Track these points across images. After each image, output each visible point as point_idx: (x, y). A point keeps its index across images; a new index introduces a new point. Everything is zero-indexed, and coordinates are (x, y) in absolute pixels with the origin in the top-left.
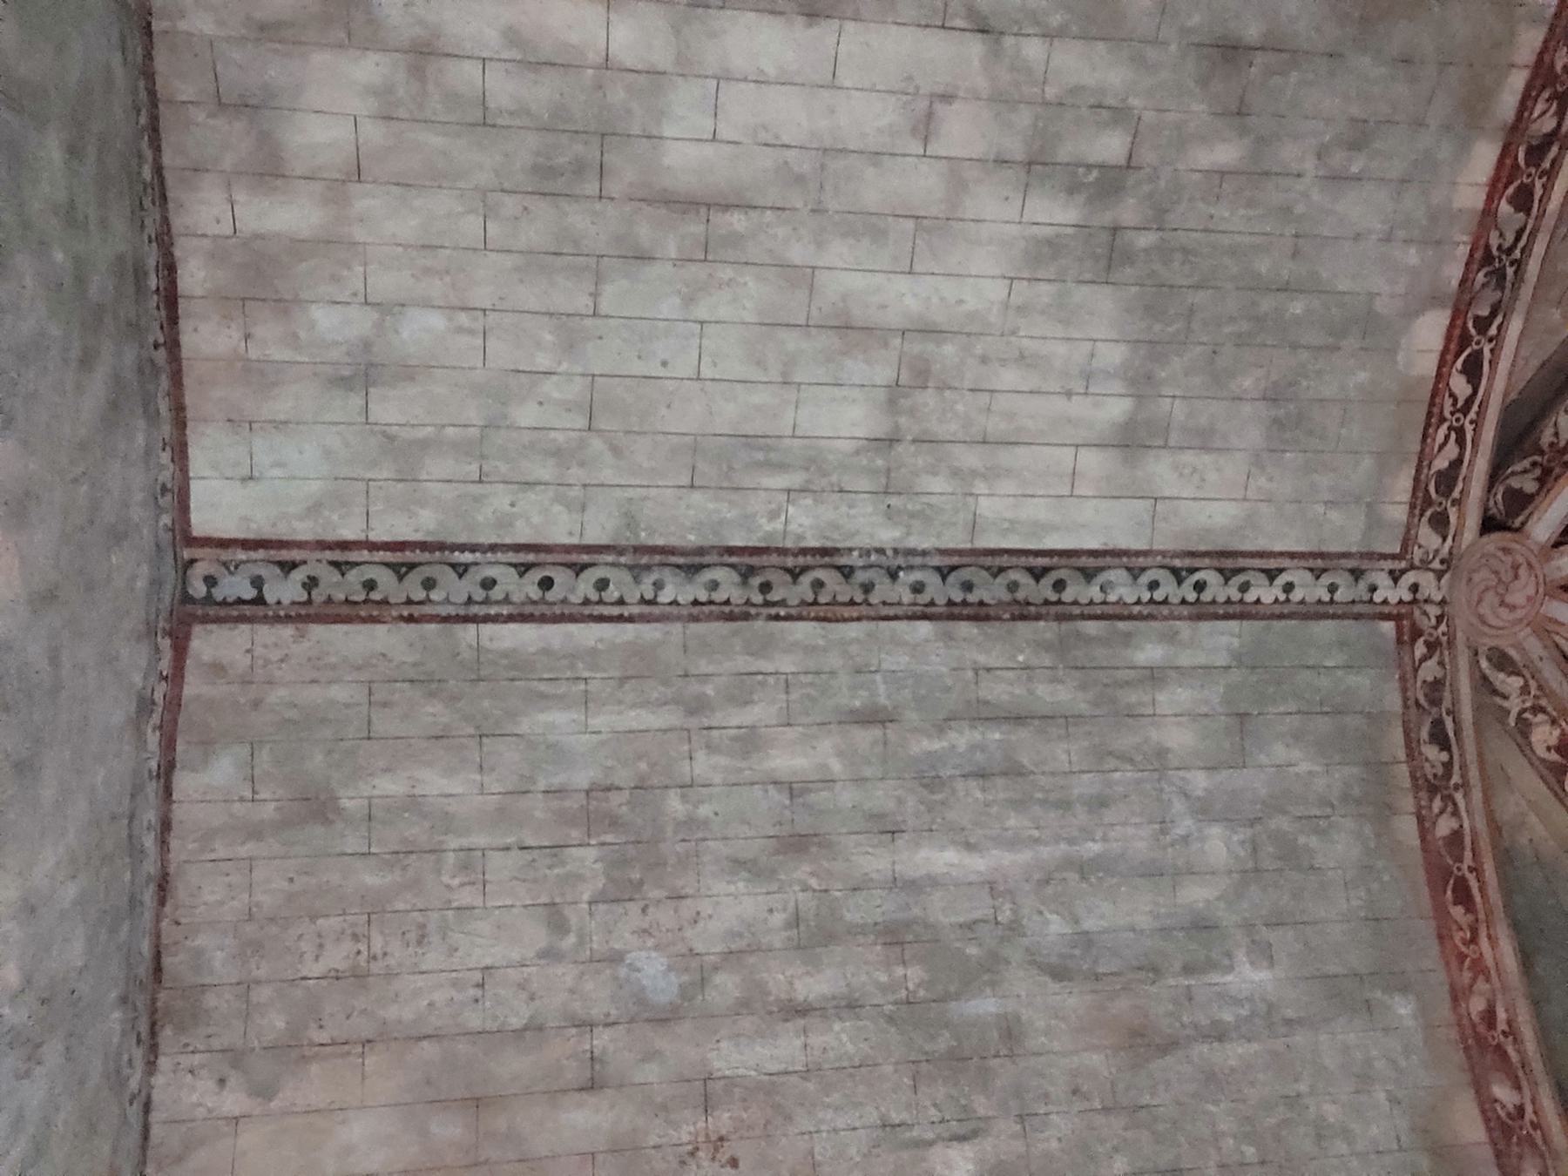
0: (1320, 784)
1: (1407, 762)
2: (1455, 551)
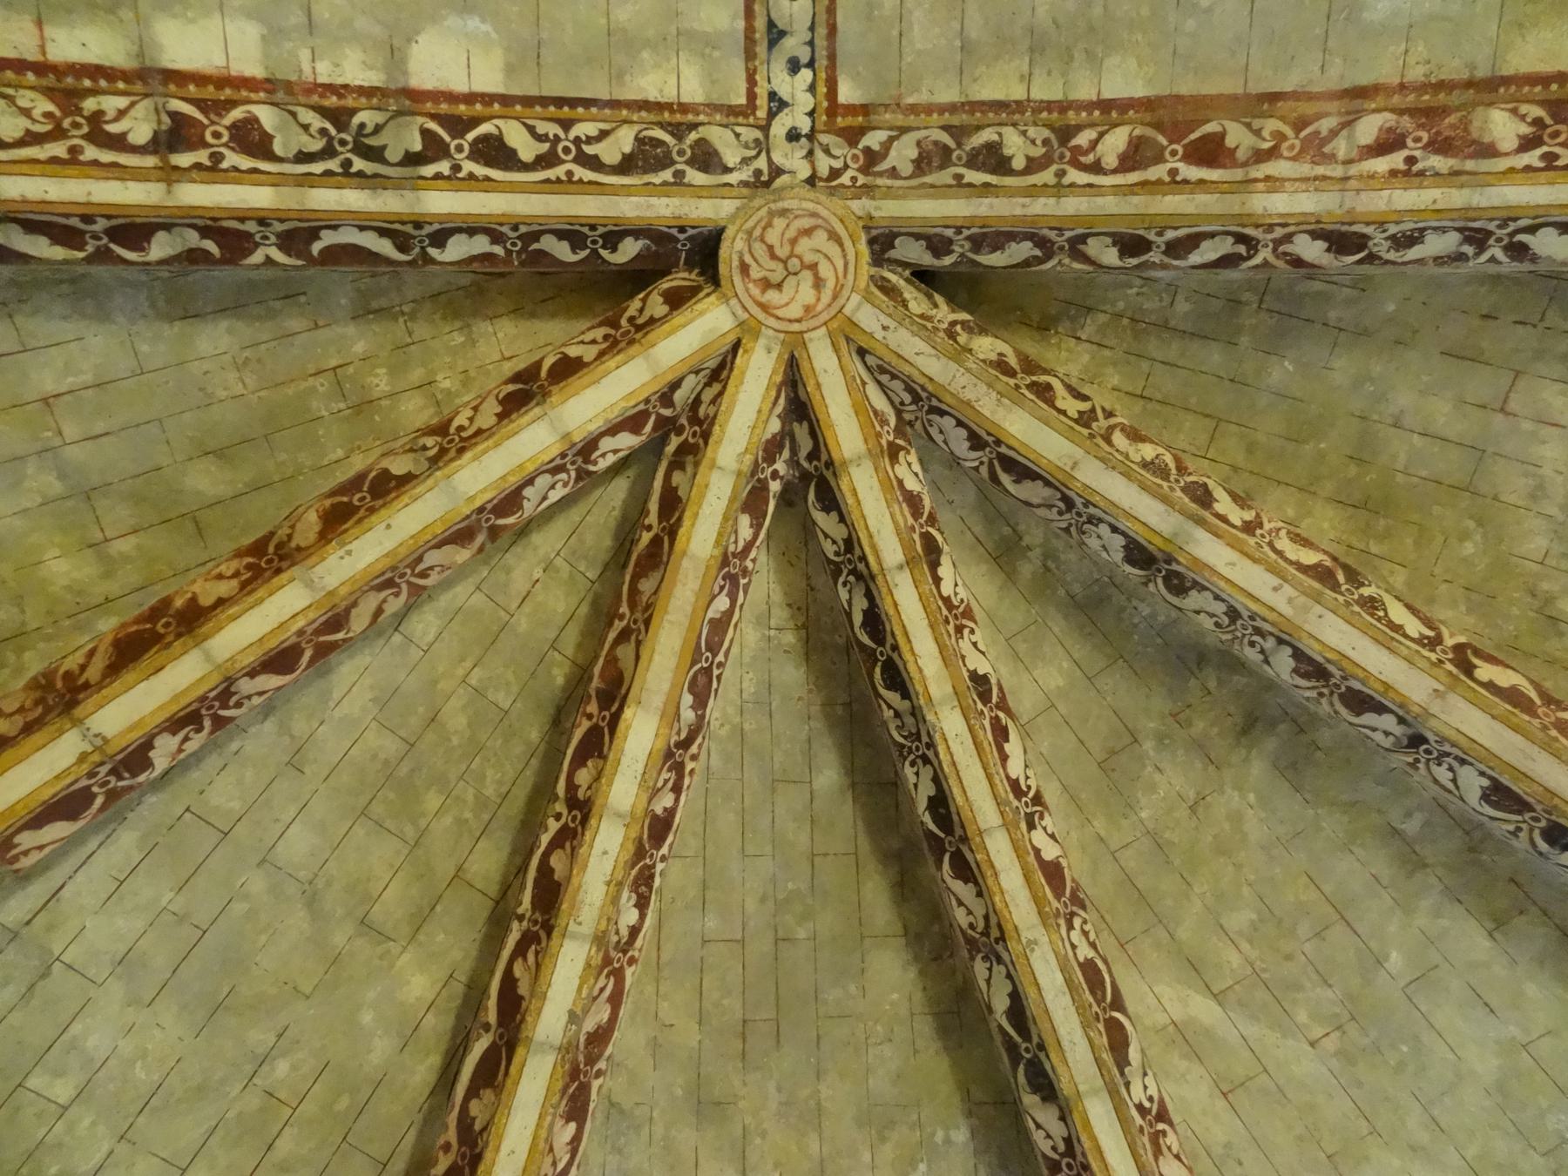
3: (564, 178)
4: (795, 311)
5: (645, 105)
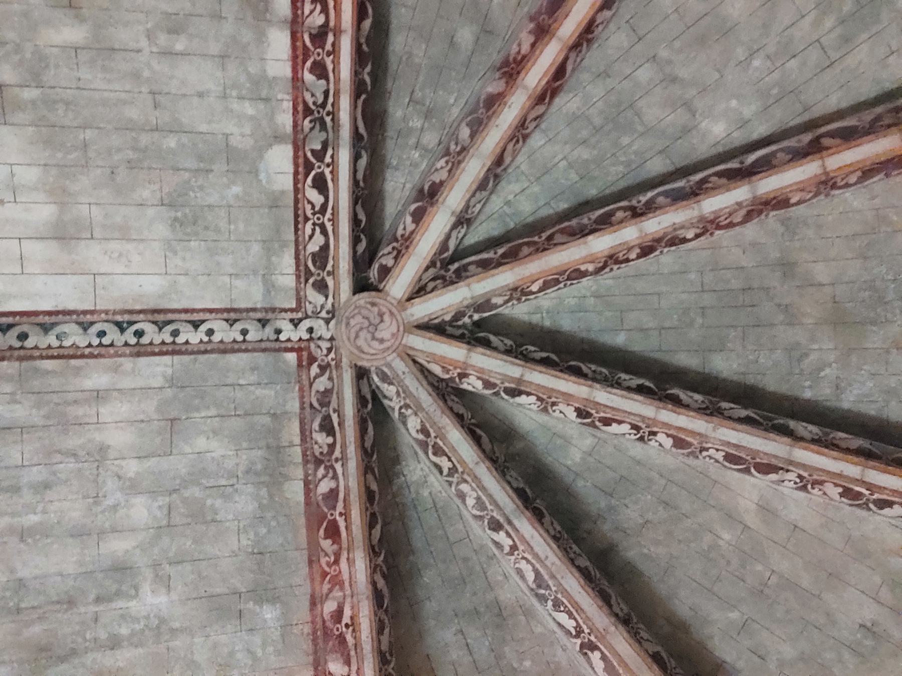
0: (229, 464)
1: (301, 445)
2: (336, 305)
3: (331, 223)
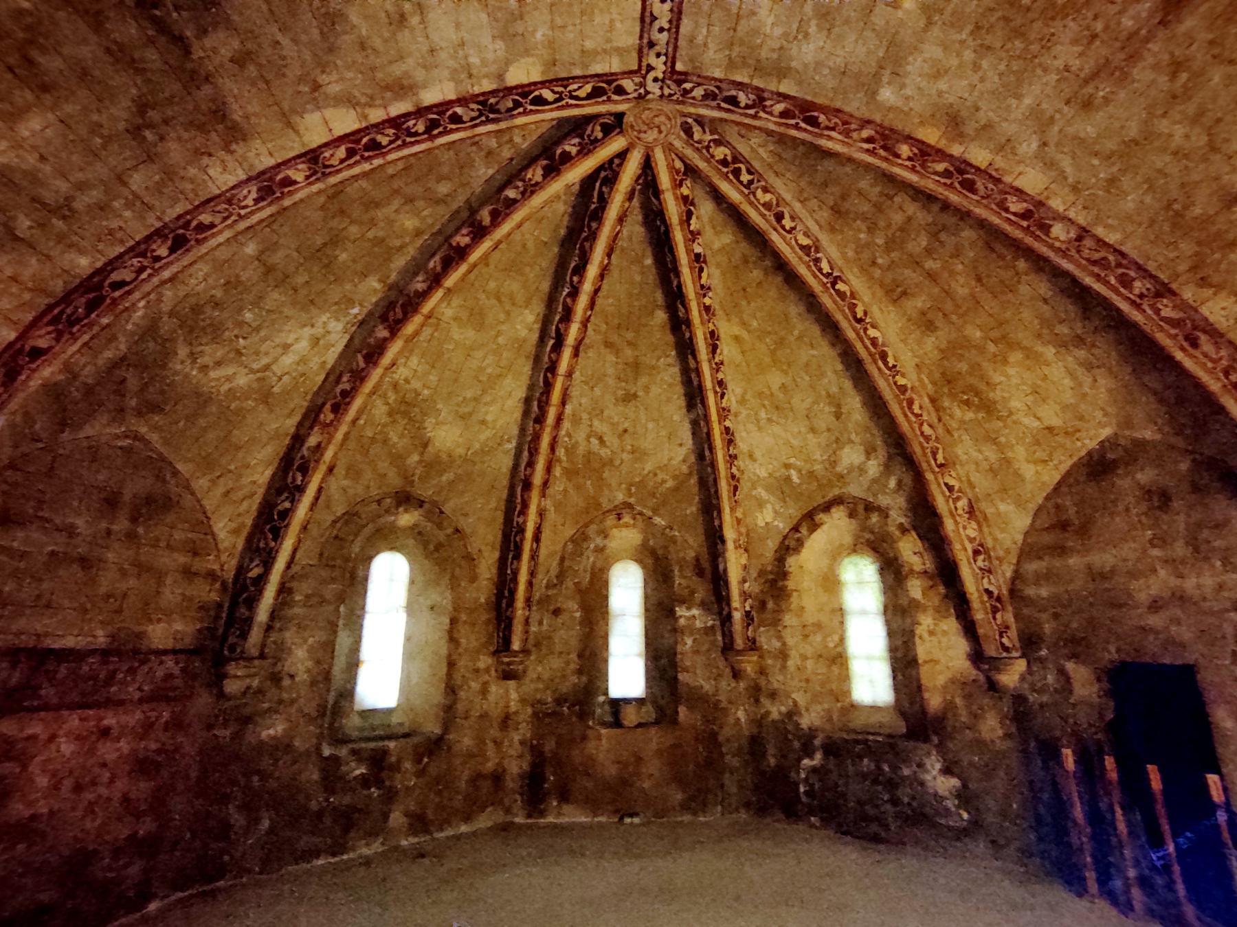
4: (650, 139)
5: (597, 75)
